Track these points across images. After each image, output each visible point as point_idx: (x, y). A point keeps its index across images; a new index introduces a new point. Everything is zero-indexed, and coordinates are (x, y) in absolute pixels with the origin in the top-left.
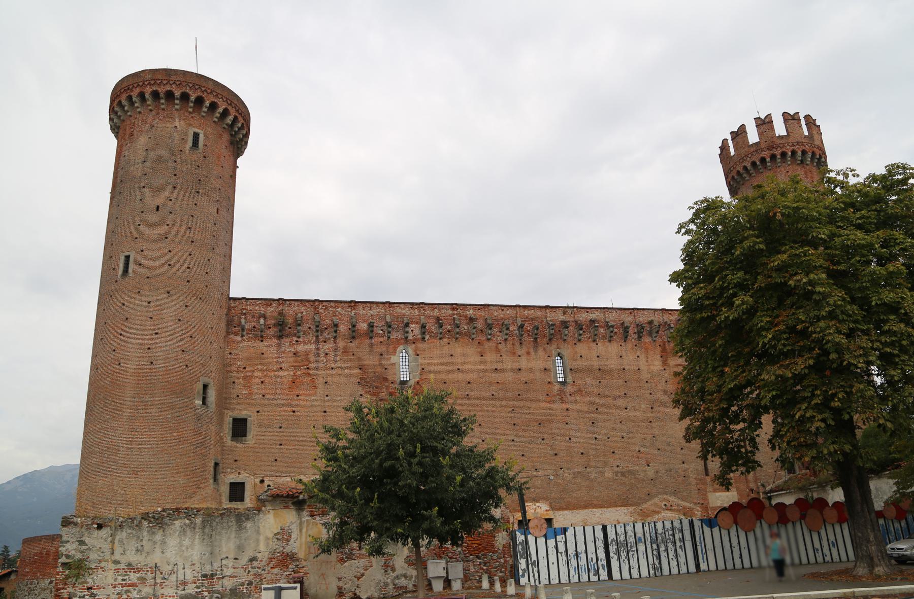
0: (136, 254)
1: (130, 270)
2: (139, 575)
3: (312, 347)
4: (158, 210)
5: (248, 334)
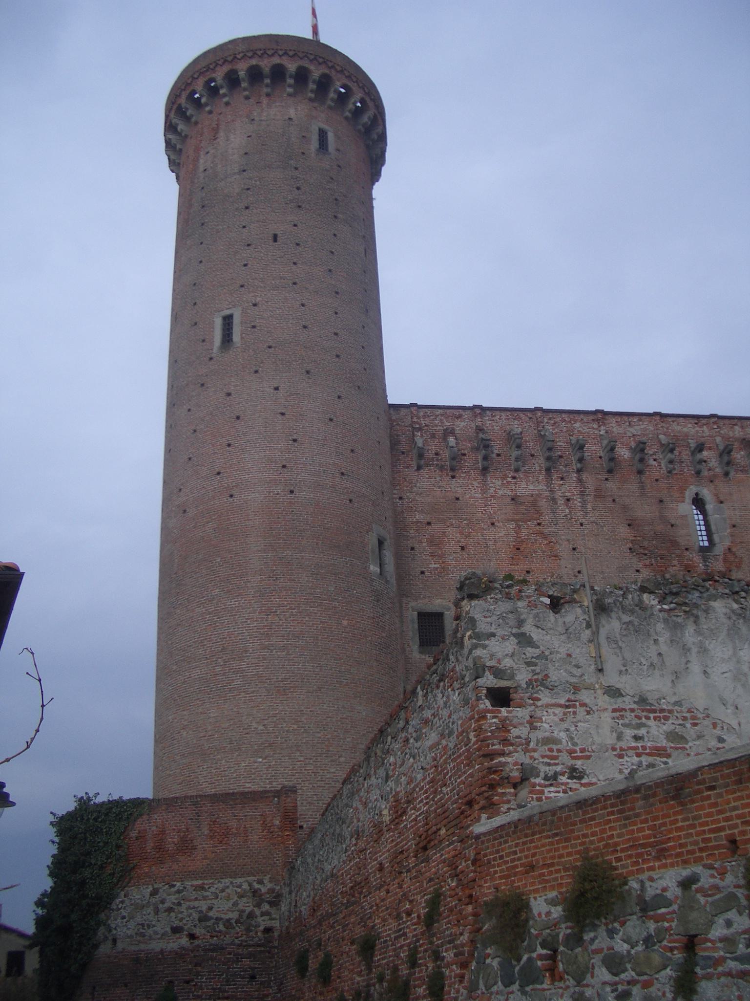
1: (236, 337)
2: (668, 727)
3: (542, 487)
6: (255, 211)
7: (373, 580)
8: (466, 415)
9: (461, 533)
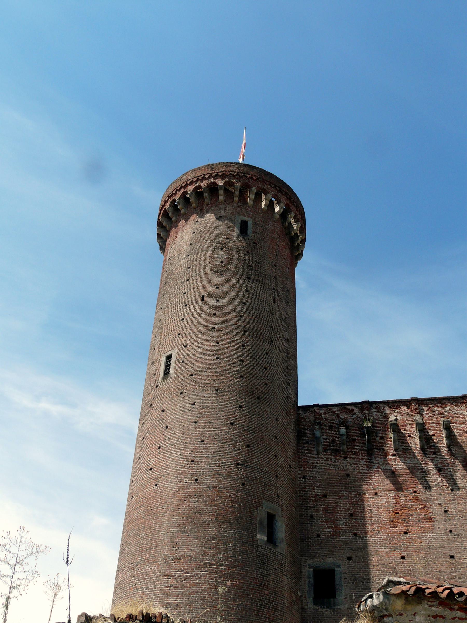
0: (178, 352)
1: (172, 371)
4: (203, 300)
5: (325, 450)
6: (192, 282)
7: (258, 547)
8: (357, 409)
9: (351, 502)
